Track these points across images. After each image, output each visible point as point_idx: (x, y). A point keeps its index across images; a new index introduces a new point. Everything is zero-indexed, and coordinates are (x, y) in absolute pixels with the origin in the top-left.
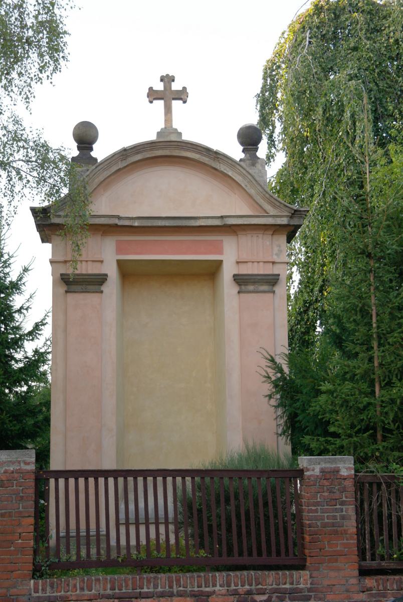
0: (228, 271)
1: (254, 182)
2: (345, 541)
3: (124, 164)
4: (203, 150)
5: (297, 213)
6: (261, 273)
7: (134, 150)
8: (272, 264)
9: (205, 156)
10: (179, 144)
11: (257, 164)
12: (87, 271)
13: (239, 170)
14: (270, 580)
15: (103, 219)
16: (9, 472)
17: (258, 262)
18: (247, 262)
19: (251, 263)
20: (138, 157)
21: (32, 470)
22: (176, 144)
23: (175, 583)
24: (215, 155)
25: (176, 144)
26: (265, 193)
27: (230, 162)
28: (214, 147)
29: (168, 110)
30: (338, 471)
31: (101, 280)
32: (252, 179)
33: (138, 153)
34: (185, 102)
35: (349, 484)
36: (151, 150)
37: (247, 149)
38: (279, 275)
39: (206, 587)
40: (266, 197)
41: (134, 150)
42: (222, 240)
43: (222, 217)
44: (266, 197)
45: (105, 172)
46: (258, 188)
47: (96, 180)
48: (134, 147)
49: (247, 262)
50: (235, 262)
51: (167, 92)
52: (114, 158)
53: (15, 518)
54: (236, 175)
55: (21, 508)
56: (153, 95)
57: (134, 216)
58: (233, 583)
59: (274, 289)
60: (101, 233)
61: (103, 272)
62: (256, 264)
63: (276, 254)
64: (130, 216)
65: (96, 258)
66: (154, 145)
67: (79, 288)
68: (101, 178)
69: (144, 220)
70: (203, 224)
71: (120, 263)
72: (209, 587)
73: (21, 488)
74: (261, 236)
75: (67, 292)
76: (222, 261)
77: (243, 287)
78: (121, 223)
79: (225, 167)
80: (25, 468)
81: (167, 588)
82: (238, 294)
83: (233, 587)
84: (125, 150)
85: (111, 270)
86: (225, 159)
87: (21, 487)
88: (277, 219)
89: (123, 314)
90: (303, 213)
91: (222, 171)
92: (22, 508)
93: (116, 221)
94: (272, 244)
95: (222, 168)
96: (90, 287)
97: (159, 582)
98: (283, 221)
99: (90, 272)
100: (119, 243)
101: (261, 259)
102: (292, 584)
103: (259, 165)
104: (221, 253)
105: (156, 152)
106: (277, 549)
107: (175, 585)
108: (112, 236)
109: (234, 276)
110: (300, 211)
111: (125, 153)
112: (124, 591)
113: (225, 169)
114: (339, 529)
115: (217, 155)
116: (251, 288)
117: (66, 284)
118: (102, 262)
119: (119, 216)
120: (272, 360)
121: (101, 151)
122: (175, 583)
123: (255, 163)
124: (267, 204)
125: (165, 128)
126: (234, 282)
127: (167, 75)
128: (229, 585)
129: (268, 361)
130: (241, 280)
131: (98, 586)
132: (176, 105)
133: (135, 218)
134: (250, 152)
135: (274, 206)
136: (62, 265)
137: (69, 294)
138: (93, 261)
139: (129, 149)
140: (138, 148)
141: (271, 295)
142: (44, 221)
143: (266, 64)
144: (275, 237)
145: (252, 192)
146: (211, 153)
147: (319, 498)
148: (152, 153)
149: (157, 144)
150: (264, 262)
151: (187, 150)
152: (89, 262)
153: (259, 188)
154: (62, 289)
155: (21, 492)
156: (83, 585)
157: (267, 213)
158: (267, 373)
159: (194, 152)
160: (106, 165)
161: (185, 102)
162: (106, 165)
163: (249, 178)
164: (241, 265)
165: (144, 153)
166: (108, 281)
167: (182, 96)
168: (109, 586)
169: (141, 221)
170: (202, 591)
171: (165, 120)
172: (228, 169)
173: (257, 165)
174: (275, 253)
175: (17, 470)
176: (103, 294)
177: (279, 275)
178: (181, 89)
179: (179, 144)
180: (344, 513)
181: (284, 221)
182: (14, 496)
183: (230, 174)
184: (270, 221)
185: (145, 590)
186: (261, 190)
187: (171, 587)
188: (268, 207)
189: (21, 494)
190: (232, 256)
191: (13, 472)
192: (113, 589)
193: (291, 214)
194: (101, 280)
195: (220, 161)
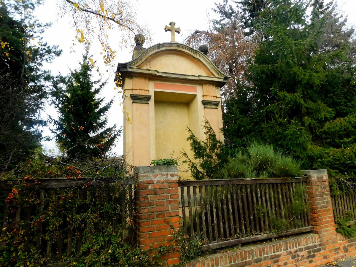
0: (199, 99)
2: (329, 215)
14: (303, 243)
16: (160, 182)
19: (138, 90)
21: (176, 180)
23: (262, 252)
30: (322, 178)
33: (164, 47)
34: (179, 33)
35: (327, 184)
36: (169, 46)
38: (151, 96)
39: (277, 252)
43: (199, 76)
53: (167, 218)
55: (170, 210)
56: (167, 30)
58: (289, 247)
65: (146, 89)
67: (138, 101)
71: (155, 92)
72: (278, 252)
73: (169, 194)
78: (158, 74)
80: (171, 179)
81: (259, 256)
83: (289, 250)
84: (160, 44)
85: (152, 94)
87: (169, 193)
92: (171, 210)
93: (156, 73)
96: (143, 102)
97: (255, 253)
102: (313, 243)
104: (196, 92)
106: (219, 221)
107: (262, 254)
109: (202, 101)
112: (237, 262)
114: (326, 209)
116: (209, 106)
118: (148, 91)
121: (146, 45)
122: (262, 252)
128: (287, 249)
131: (222, 262)
135: (218, 74)
136: (131, 91)
137: (134, 104)
138: (145, 90)
140: (164, 44)
145: (209, 67)
147: (165, 202)
155: (170, 198)
156: (213, 262)
168: (228, 261)
170: (275, 255)
175: (166, 180)
180: (327, 200)
182: (165, 201)
183: (201, 59)
185: (248, 260)
187: (260, 255)
189: (170, 199)
190: (200, 92)
191: (163, 183)
192: (230, 262)
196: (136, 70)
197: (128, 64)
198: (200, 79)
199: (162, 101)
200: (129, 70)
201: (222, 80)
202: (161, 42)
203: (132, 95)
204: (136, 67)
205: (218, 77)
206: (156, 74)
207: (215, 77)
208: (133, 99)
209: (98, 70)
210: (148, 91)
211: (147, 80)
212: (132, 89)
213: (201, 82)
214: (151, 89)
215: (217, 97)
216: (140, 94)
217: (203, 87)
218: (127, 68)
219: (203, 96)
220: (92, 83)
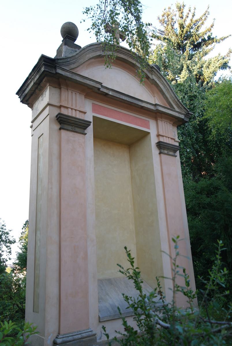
0: (154, 140)
1: (170, 91)
26: (175, 98)
32: (169, 89)
43: (156, 105)
45: (93, 53)
47: (88, 56)
54: (160, 84)
60: (85, 94)
67: (70, 128)
82: (159, 155)
96: (77, 129)
105: (120, 54)
108: (128, 74)
113: (155, 79)
126: (156, 147)
135: (179, 107)
137: (62, 131)
142: (50, 70)
148: (118, 54)
153: (172, 94)
154: (57, 127)
160: (95, 48)
162: (95, 48)
163: (167, 88)
172: (157, 79)
186: (173, 96)
196: (71, 74)
197: (59, 61)
200: (59, 71)
201: (182, 117)
204: (70, 69)
205: (178, 111)
207: (172, 109)
208: (60, 124)
209: (10, 231)
211: (83, 97)
214: (86, 110)
218: (55, 68)
220: (228, 66)
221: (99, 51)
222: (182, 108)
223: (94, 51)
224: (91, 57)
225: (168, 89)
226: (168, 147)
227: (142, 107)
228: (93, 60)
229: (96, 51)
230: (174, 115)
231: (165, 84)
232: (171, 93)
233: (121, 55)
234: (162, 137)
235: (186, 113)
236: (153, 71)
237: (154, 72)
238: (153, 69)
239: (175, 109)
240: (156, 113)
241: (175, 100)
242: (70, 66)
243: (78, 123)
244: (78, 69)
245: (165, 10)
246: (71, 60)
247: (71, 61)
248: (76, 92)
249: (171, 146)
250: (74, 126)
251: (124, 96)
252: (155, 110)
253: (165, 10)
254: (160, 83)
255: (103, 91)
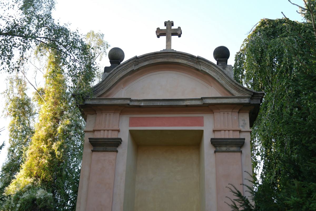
3: (137, 67)
4: (189, 57)
5: (255, 95)
6: (231, 137)
7: (143, 58)
8: (238, 132)
9: (190, 61)
10: (173, 54)
11: (226, 68)
12: (108, 136)
13: (213, 68)
15: (120, 101)
17: (229, 131)
18: (220, 131)
19: (223, 131)
20: (146, 63)
22: (171, 54)
24: (197, 60)
25: (171, 54)
27: (207, 63)
28: (196, 54)
29: (169, 41)
31: (116, 143)
32: (222, 74)
34: (180, 36)
36: (155, 58)
37: (219, 60)
38: (244, 139)
40: (233, 85)
41: (143, 58)
42: (203, 117)
43: (202, 99)
44: (233, 85)
45: (123, 72)
46: (227, 79)
48: (143, 56)
49: (220, 131)
50: (212, 130)
51: (168, 30)
52: (129, 63)
54: (211, 72)
56: (160, 33)
57: (141, 99)
59: (241, 150)
60: (120, 112)
61: (119, 137)
62: (227, 132)
63: (242, 126)
64: (139, 99)
65: (116, 128)
66: (157, 55)
67: (101, 148)
68: (121, 75)
69: (147, 102)
70: (188, 104)
71: (132, 133)
74: (230, 113)
75: (93, 151)
76: (202, 131)
77: (218, 148)
78: (132, 104)
79: (204, 67)
84: (136, 58)
85: (125, 137)
86: (204, 62)
88: (241, 99)
89: (133, 172)
90: (260, 95)
91: (202, 70)
93: (128, 102)
94: (238, 118)
95: (202, 68)
96: (109, 148)
98: (245, 100)
99: (109, 137)
100: (131, 119)
101: (231, 128)
103: (228, 69)
105: (158, 60)
110: (258, 94)
111: (137, 60)
113: (204, 69)
115: (199, 60)
116: (224, 149)
117: (93, 146)
119: (130, 98)
120: (239, 195)
123: (226, 68)
124: (233, 90)
125: (166, 49)
127: (169, 21)
129: (235, 194)
130: (215, 143)
132: (174, 38)
133: (141, 100)
134: (222, 62)
136: (92, 133)
137: (94, 153)
138: (113, 130)
139: (140, 57)
140: (146, 57)
141: (239, 154)
143: (236, 54)
144: (241, 114)
145: (223, 82)
146: (194, 59)
149: (159, 55)
150: (234, 131)
151: (179, 58)
152: (109, 131)
153: (227, 79)
157: (234, 96)
158: (235, 204)
159: (183, 59)
161: (180, 36)
163: (220, 73)
164: (216, 132)
165: (150, 61)
166: (121, 145)
167: (178, 33)
169: (145, 102)
171: (166, 45)
172: (206, 69)
173: (226, 69)
174: (241, 125)
176: (118, 153)
177: (244, 139)
178: (177, 28)
179: (173, 54)
181: (247, 101)
183: (207, 71)
184: (236, 101)
186: (229, 80)
188: (234, 92)
190: (209, 126)
193: (251, 96)
194: (116, 143)
195: (200, 64)
196: (98, 101)
198: (204, 104)
199: (143, 143)
202: (139, 54)
203: (91, 140)
206: (129, 104)
208: (215, 147)
210: (119, 131)
211: (118, 115)
212: (94, 131)
213: (207, 107)
214: (123, 127)
215: (240, 131)
216: (110, 137)
217: (214, 117)
219: (214, 131)
221: (130, 68)
222: (244, 91)
223: (124, 70)
224: (121, 76)
225: (221, 74)
226: (224, 143)
227: (187, 106)
228: (129, 76)
229: (127, 69)
230: (226, 102)
231: (217, 71)
232: (226, 77)
233: (159, 59)
234: (220, 132)
235: (250, 95)
236: (199, 61)
237: (201, 62)
238: (199, 60)
239: (234, 94)
240: (208, 106)
241: (232, 84)
242: (98, 93)
243: (108, 142)
244: (108, 93)
245: (69, 29)
246: (98, 88)
247: (98, 89)
248: (110, 113)
249: (230, 141)
250: (106, 146)
251: (159, 102)
252: (202, 104)
253: (69, 29)
254: (212, 70)
255: (134, 104)
